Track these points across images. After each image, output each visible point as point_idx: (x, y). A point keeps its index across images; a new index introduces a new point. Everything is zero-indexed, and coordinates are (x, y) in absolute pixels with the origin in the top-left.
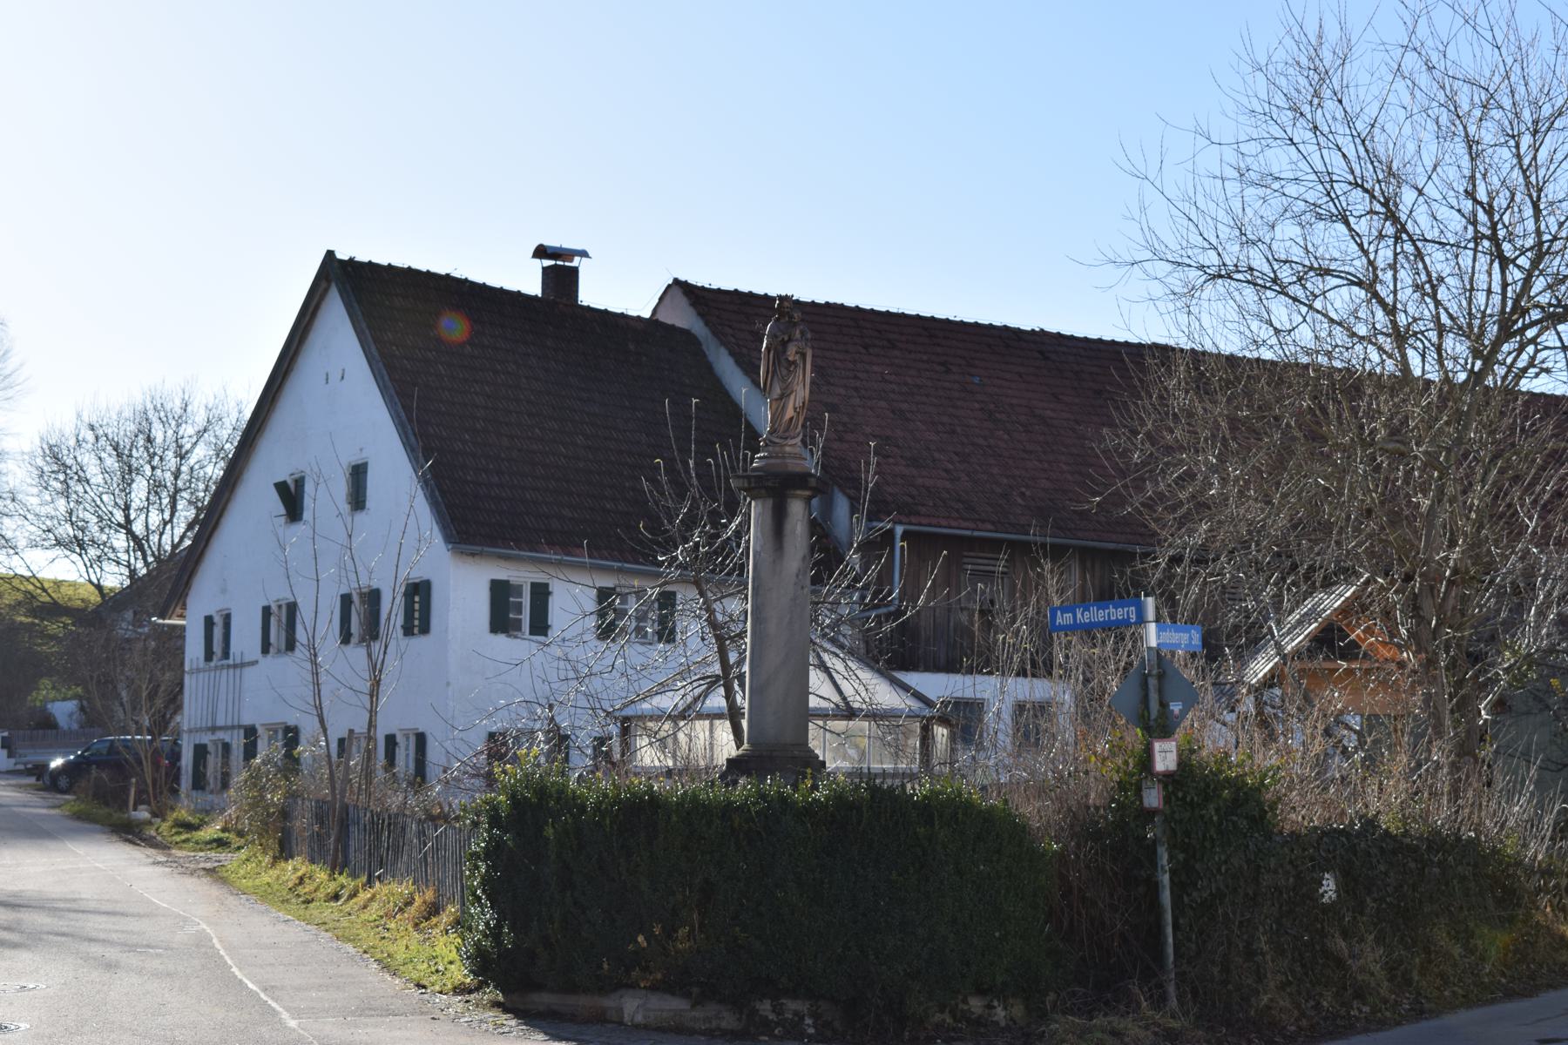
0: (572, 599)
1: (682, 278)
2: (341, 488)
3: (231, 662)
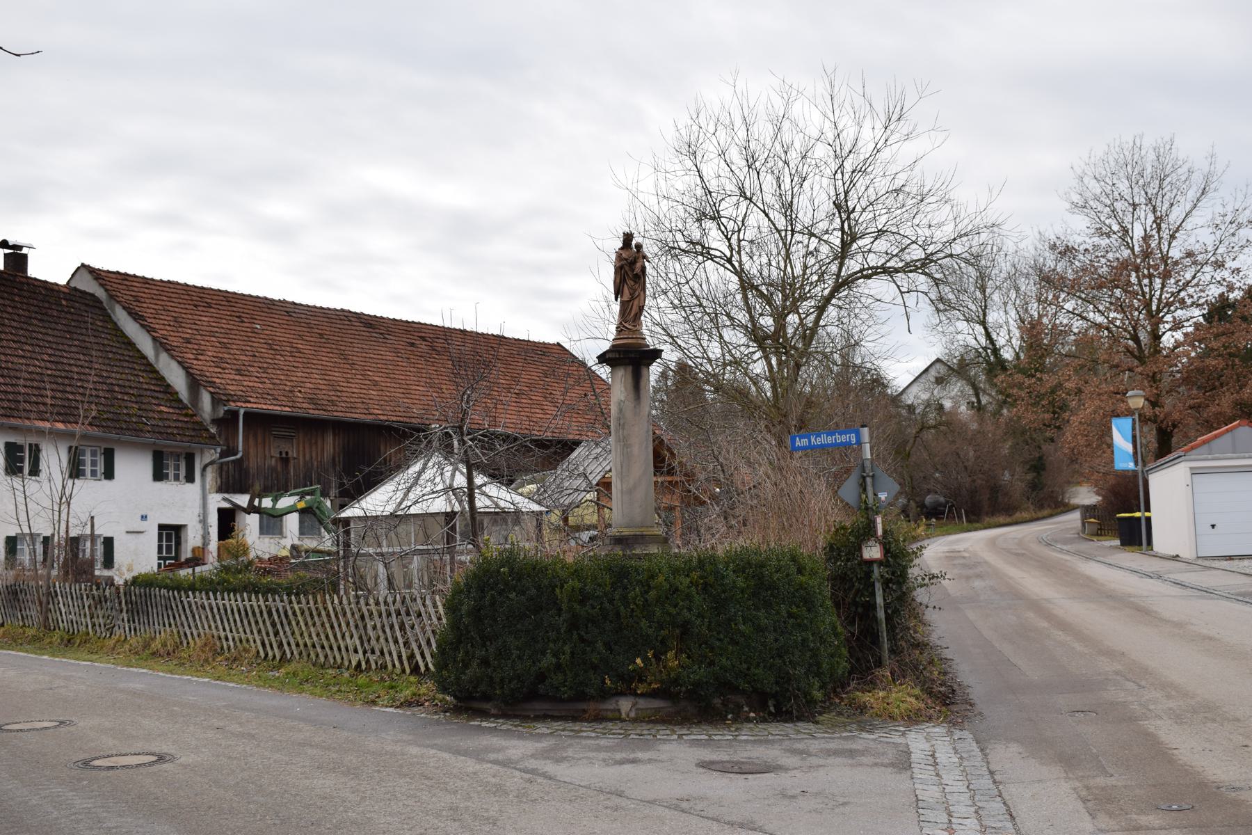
0: (54, 460)
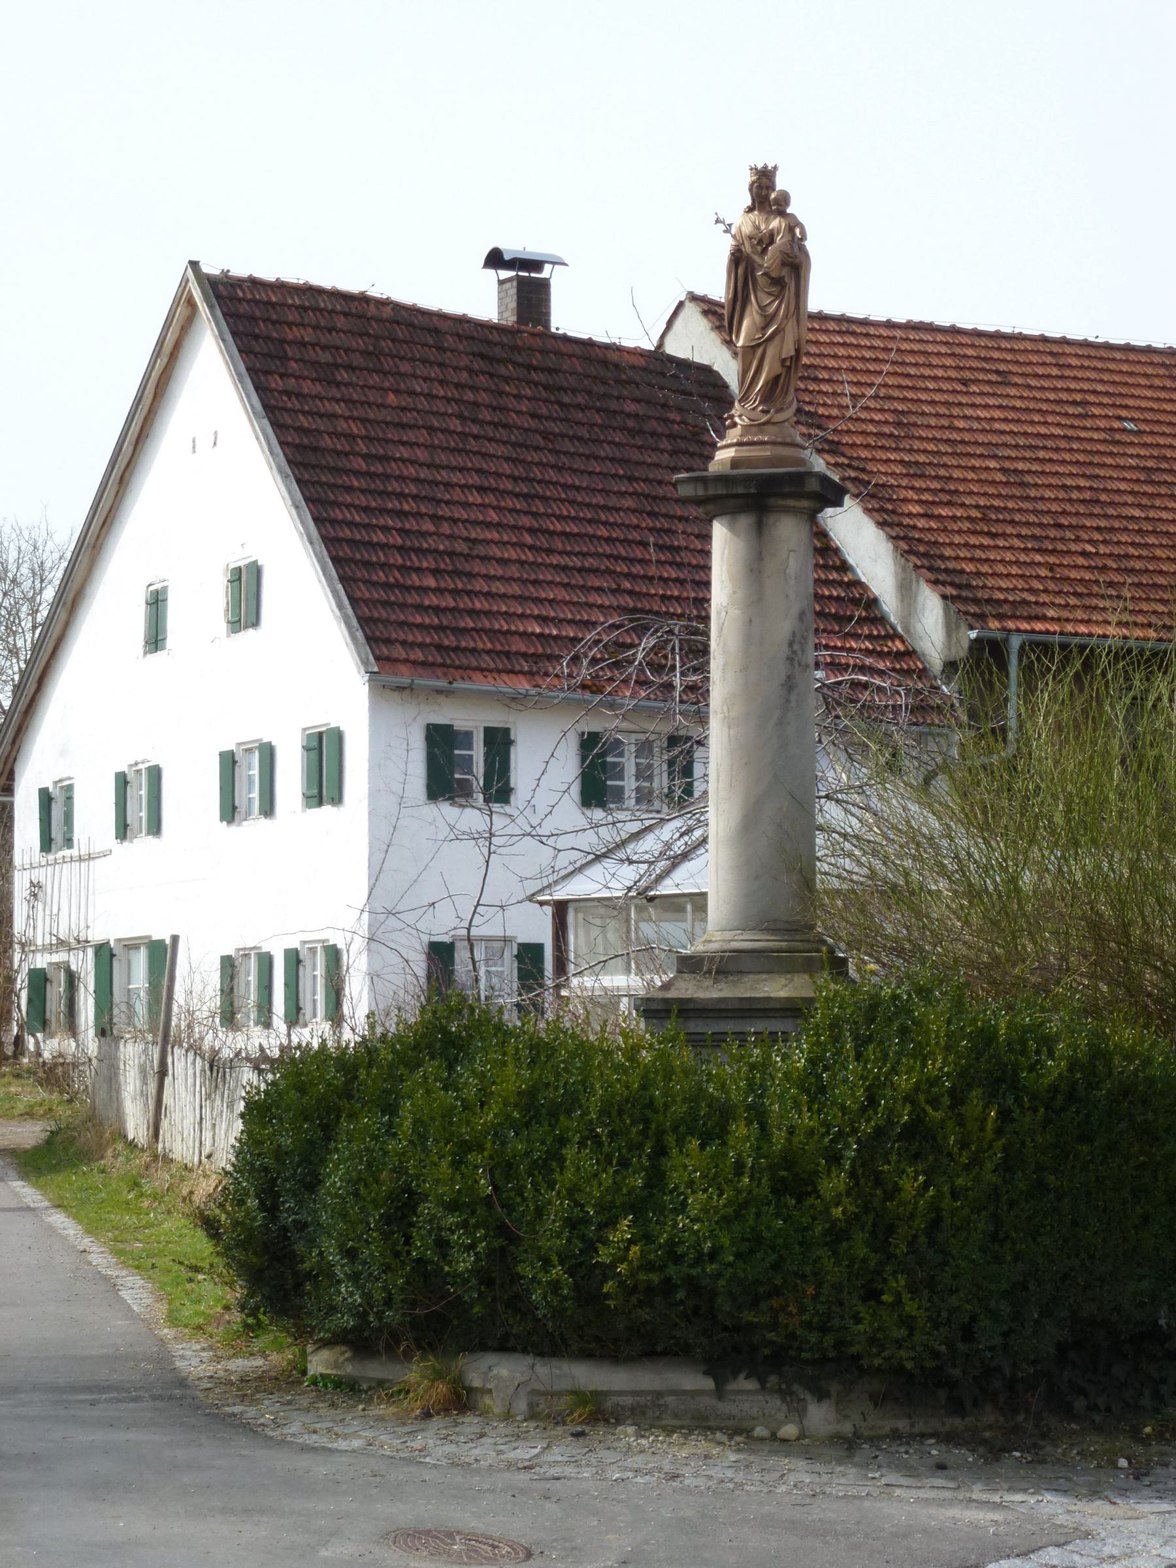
0: (545, 762)
1: (700, 292)
2: (215, 597)
3: (74, 852)
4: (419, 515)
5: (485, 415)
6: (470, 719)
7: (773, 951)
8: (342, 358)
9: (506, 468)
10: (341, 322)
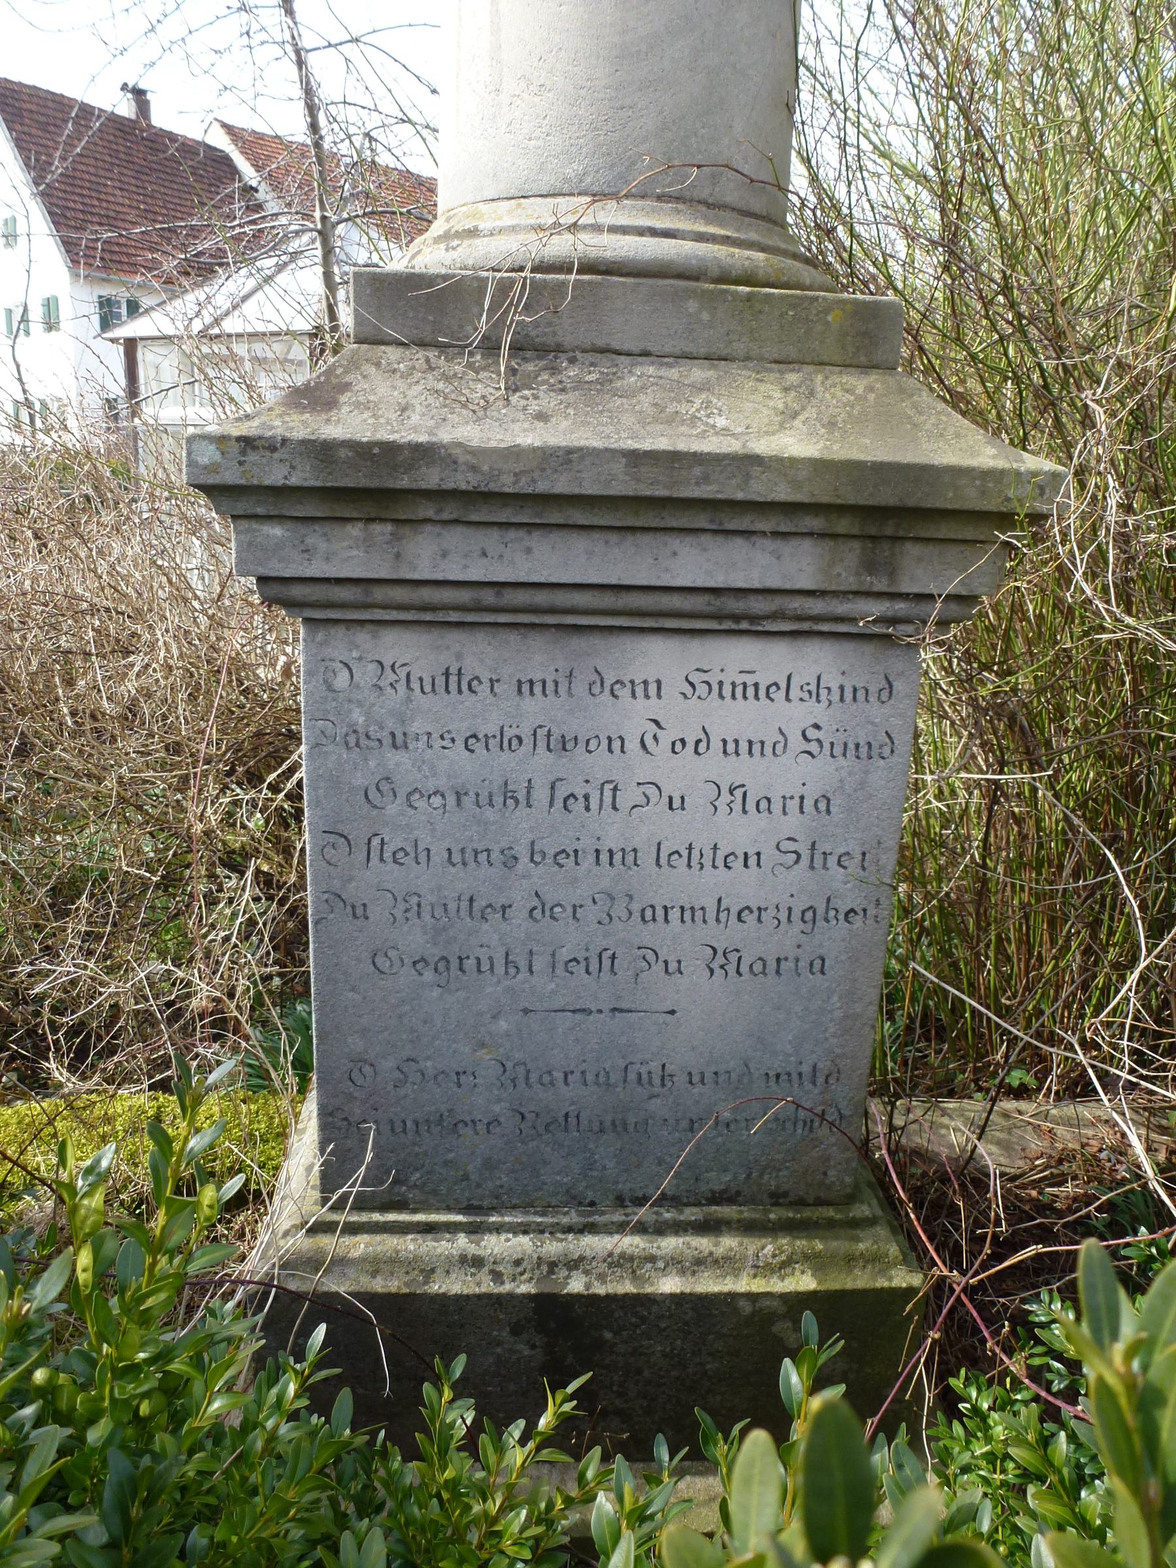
4: (90, 197)
5: (122, 156)
6: (121, 294)
7: (725, 277)
8: (52, 121)
9: (133, 181)
10: (50, 104)
